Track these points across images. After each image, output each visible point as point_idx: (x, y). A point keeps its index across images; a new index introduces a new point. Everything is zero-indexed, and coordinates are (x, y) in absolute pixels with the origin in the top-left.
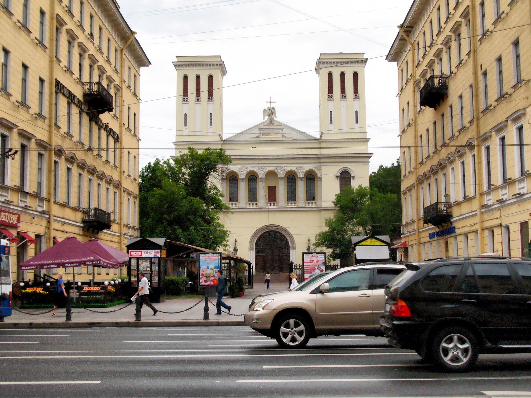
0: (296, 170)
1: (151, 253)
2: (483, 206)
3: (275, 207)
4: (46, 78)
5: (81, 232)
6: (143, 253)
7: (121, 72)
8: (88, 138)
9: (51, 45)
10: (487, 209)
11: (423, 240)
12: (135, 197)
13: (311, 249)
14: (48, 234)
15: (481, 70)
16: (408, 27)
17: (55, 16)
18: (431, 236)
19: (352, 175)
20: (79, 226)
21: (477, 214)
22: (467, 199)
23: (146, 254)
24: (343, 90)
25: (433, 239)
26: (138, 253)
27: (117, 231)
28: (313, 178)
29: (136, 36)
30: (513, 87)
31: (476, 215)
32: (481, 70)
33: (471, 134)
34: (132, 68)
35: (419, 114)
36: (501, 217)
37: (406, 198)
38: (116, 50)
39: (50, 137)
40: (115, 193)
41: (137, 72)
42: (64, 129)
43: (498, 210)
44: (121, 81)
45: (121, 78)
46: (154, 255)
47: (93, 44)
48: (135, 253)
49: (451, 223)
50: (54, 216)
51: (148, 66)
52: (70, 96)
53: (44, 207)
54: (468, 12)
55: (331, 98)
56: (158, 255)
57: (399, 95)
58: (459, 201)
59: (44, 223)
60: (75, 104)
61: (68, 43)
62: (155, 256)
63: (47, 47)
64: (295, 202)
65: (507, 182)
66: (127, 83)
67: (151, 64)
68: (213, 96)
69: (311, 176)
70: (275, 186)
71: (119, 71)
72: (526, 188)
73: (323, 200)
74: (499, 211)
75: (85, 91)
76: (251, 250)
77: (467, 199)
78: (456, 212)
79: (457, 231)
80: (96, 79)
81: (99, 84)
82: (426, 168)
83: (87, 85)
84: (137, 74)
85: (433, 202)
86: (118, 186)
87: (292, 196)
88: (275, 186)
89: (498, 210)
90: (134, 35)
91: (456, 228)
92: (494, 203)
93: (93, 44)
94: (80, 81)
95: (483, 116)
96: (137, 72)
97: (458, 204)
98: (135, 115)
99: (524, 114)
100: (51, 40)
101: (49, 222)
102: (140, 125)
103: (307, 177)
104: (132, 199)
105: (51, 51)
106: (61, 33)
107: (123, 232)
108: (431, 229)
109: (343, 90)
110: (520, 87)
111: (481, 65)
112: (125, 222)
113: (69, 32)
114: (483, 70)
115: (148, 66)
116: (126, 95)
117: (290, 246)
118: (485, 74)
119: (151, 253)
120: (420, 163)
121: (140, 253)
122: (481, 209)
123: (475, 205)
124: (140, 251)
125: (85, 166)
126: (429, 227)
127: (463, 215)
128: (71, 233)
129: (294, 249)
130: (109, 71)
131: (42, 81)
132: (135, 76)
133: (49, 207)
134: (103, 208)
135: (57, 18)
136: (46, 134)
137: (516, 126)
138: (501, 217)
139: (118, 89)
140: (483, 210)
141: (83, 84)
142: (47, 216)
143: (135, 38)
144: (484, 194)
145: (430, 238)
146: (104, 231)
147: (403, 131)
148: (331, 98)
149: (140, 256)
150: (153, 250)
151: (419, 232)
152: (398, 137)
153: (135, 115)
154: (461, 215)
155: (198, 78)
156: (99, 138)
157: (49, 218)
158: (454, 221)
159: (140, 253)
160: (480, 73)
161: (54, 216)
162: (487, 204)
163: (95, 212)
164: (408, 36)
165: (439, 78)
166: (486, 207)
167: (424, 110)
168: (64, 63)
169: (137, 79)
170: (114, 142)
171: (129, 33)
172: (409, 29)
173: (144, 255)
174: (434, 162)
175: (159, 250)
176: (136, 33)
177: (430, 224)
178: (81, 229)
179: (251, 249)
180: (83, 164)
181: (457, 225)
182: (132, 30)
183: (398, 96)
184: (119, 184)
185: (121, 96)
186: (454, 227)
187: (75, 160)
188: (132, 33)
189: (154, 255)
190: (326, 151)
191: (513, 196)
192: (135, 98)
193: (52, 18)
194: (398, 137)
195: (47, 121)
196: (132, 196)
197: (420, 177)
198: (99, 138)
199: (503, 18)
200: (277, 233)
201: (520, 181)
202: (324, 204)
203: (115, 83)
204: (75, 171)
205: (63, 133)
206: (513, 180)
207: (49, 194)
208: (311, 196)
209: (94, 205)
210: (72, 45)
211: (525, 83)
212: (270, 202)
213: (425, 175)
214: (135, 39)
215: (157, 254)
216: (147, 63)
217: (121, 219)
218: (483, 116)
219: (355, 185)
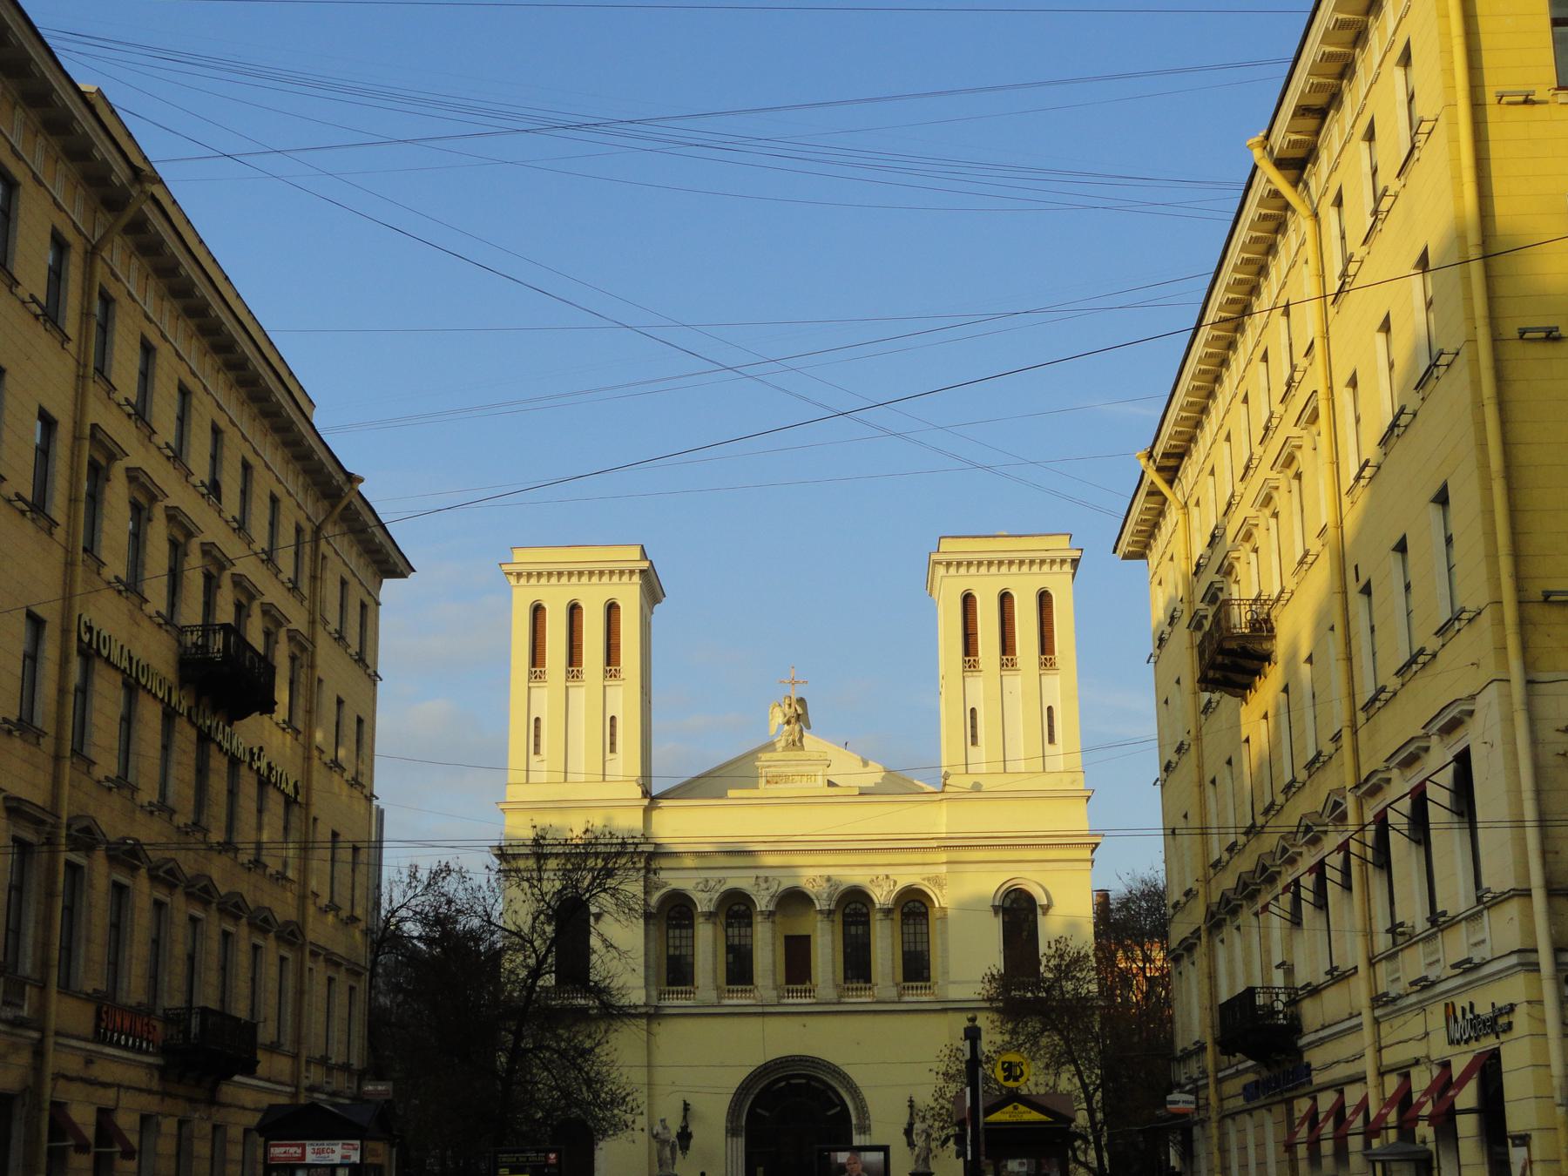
0: (869, 885)
1: (333, 1152)
2: (1378, 1000)
3: (808, 1000)
4: (50, 613)
5: (155, 1085)
6: (309, 1149)
7: (313, 591)
8: (190, 793)
9: (71, 517)
10: (1390, 1008)
11: (1231, 1104)
12: (354, 972)
13: (915, 1132)
14: (32, 1091)
15: (1358, 580)
16: (1165, 455)
17: (87, 431)
18: (1250, 1092)
19: (1042, 899)
20: (149, 1065)
21: (1361, 1024)
22: (1338, 976)
23: (319, 1152)
24: (1007, 645)
25: (1256, 1104)
26: (292, 1150)
27: (286, 1078)
28: (923, 910)
29: (361, 487)
30: (1441, 632)
31: (1359, 1026)
32: (1358, 580)
33: (1340, 775)
34: (353, 582)
35: (1206, 713)
36: (1427, 1034)
37: (1180, 973)
38: (299, 530)
39: (55, 796)
40: (283, 959)
41: (369, 593)
42: (107, 766)
43: (1416, 1012)
44: (312, 623)
45: (312, 613)
46: (344, 1157)
47: (220, 512)
48: (282, 1150)
49: (1299, 1052)
50: (57, 1034)
51: (403, 575)
52: (131, 664)
53: (26, 1007)
54: (1316, 409)
55: (972, 669)
56: (355, 1158)
57: (1155, 659)
58: (1315, 983)
59: (24, 1058)
60: (149, 691)
61: (132, 510)
62: (346, 1161)
63: (57, 520)
64: (868, 985)
65: (1438, 921)
66: (334, 625)
67: (414, 571)
68: (581, 666)
69: (917, 904)
70: (809, 936)
71: (305, 591)
72: (1488, 941)
73: (952, 977)
74: (1421, 1017)
75: (185, 652)
76: (733, 1135)
77: (1338, 976)
78: (1312, 1013)
79: (1318, 1079)
80: (225, 613)
81: (233, 632)
82: (1228, 881)
83: (192, 632)
84: (368, 600)
85: (1240, 989)
86: (292, 935)
87: (857, 966)
88: (809, 936)
89: (1416, 1012)
90: (355, 485)
91: (1313, 1066)
92: (1409, 991)
93: (220, 512)
94: (168, 621)
95: (1368, 720)
96: (369, 593)
97: (1314, 991)
98: (360, 721)
99: (1471, 713)
100: (73, 500)
101: (39, 1052)
102: (377, 751)
103: (906, 910)
104: (342, 979)
105: (71, 534)
106: (108, 480)
107: (305, 1083)
108: (1246, 1070)
109: (1007, 645)
110: (1459, 630)
111: (1356, 567)
112: (314, 1046)
113: (133, 475)
114: (1363, 581)
115: (406, 577)
116: (330, 661)
117: (854, 1121)
118: (1367, 590)
119: (333, 1152)
120: (1211, 866)
121: (299, 1151)
122: (1373, 1010)
123: (1359, 992)
124: (298, 1146)
125: (178, 879)
126: (1241, 1067)
127: (1330, 1026)
128: (119, 1086)
129: (864, 1133)
130: (273, 593)
131: (36, 622)
132: (363, 606)
133: (42, 1008)
134: (241, 1010)
135: (93, 436)
136: (44, 780)
137: (1453, 749)
138: (1427, 1034)
139: (303, 648)
140: (1378, 1013)
141: (182, 630)
142: (35, 1035)
143: (359, 494)
144: (1460, 921)
145: (1248, 1099)
146: (237, 1078)
147: (1168, 768)
148: (972, 669)
149: (299, 1159)
150: (341, 1142)
151: (1219, 1081)
152: (1155, 784)
153: (360, 721)
154: (1324, 1027)
155: (574, 610)
156: (232, 793)
157: (41, 1041)
158: (1304, 1046)
159: (299, 1151)
160: (1353, 588)
161: (57, 1034)
162: (1386, 994)
163: (203, 1023)
164: (1170, 483)
165: (1248, 607)
166: (1386, 1004)
167: (1218, 702)
168: (116, 565)
169: (370, 615)
170: (283, 804)
171: (340, 478)
172: (1171, 463)
173: (310, 1158)
174: (1245, 863)
175: (358, 1143)
176: (362, 480)
177: (1239, 1056)
178: (156, 1074)
179: (732, 1131)
180: (170, 872)
181: (1315, 1057)
182: (349, 469)
183: (1152, 660)
184: (297, 932)
185: (312, 666)
186: (1308, 1065)
187: (139, 860)
188: (351, 479)
189: (344, 1157)
190: (1530, 812)
191: (1454, 966)
192: (360, 672)
193: (77, 438)
194: (1155, 784)
195: (47, 744)
196: (343, 968)
197: (1214, 908)
198: (232, 793)
199: (1406, 426)
200: (813, 1083)
201: (1473, 917)
202: (955, 993)
203: (292, 626)
204: (143, 891)
205: (102, 779)
206: (1454, 918)
207: (44, 964)
208: (916, 967)
209: (173, 999)
210: (144, 514)
211: (1470, 620)
212: (791, 987)
213: (1225, 900)
214: (357, 496)
215: (351, 1153)
216: (402, 566)
217: (298, 1040)
218: (1368, 720)
219: (1049, 928)
